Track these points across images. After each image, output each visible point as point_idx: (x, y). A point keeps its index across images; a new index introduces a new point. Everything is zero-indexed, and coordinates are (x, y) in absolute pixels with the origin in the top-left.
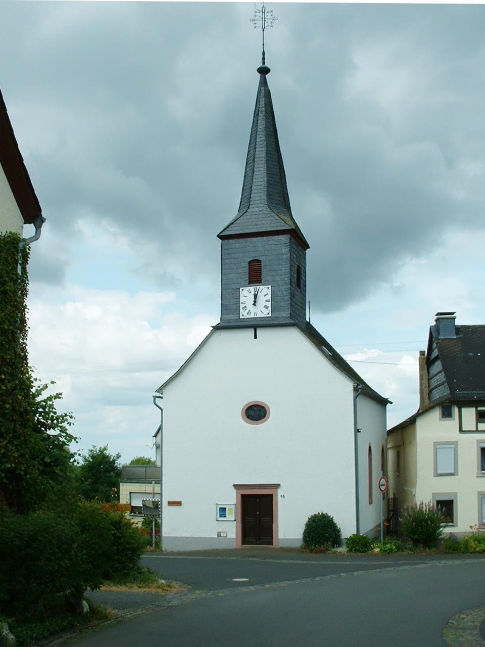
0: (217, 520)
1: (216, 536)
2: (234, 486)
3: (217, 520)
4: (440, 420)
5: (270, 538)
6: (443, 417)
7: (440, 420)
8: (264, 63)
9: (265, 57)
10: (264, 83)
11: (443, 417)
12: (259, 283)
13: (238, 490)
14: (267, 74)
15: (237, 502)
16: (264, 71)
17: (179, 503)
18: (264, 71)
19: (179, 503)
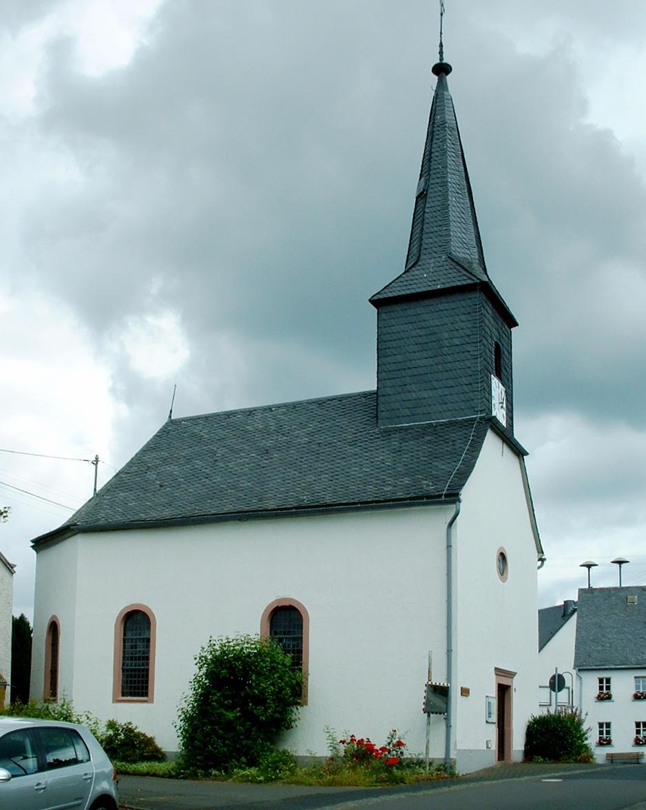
0: (487, 722)
1: (485, 748)
2: (496, 669)
3: (487, 741)
4: (116, 701)
5: (384, 338)
6: (146, 694)
7: (116, 701)
8: (441, 59)
9: (439, 56)
10: (442, 86)
11: (146, 694)
12: (142, 695)
13: (499, 677)
14: (447, 75)
15: (446, 79)
16: (442, 70)
17: (503, 557)
18: (442, 70)
19: (503, 557)
